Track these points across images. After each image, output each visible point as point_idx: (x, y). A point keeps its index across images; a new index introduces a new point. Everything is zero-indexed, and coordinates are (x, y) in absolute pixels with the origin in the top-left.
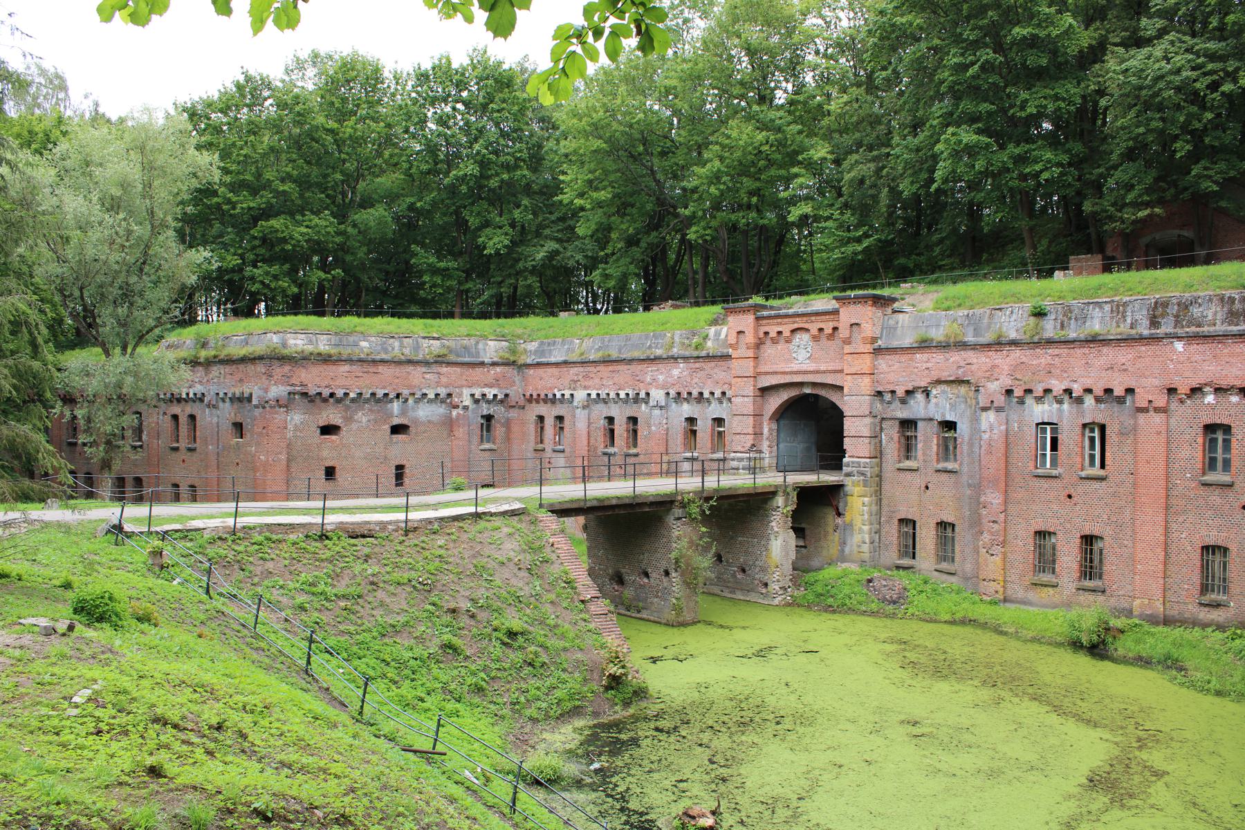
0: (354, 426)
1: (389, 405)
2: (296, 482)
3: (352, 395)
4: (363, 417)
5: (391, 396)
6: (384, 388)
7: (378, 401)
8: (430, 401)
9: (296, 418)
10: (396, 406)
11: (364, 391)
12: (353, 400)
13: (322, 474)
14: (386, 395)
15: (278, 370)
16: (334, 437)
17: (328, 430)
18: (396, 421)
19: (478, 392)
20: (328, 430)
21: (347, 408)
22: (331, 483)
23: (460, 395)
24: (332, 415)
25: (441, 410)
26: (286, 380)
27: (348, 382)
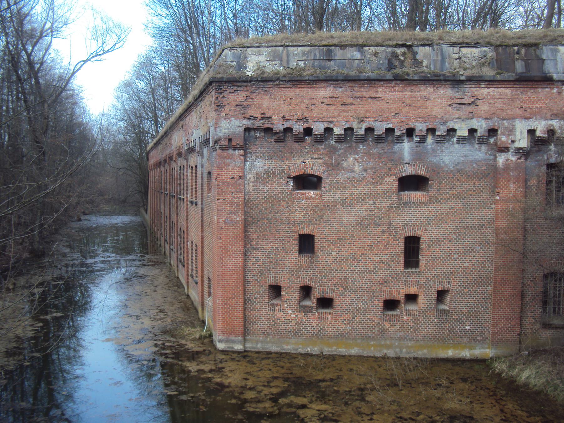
0: (342, 177)
1: (397, 147)
2: (258, 253)
3: (338, 131)
4: (355, 163)
5: (397, 133)
6: (387, 119)
7: (379, 140)
8: (462, 140)
9: (258, 164)
10: (406, 148)
11: (355, 125)
12: (340, 139)
13: (293, 245)
14: (390, 131)
15: (231, 97)
16: (312, 193)
17: (306, 182)
18: (408, 171)
19: (540, 127)
20: (306, 182)
21: (333, 150)
22: (307, 259)
23: (511, 131)
24: (309, 161)
25: (477, 154)
26: (242, 109)
27: (331, 112)
